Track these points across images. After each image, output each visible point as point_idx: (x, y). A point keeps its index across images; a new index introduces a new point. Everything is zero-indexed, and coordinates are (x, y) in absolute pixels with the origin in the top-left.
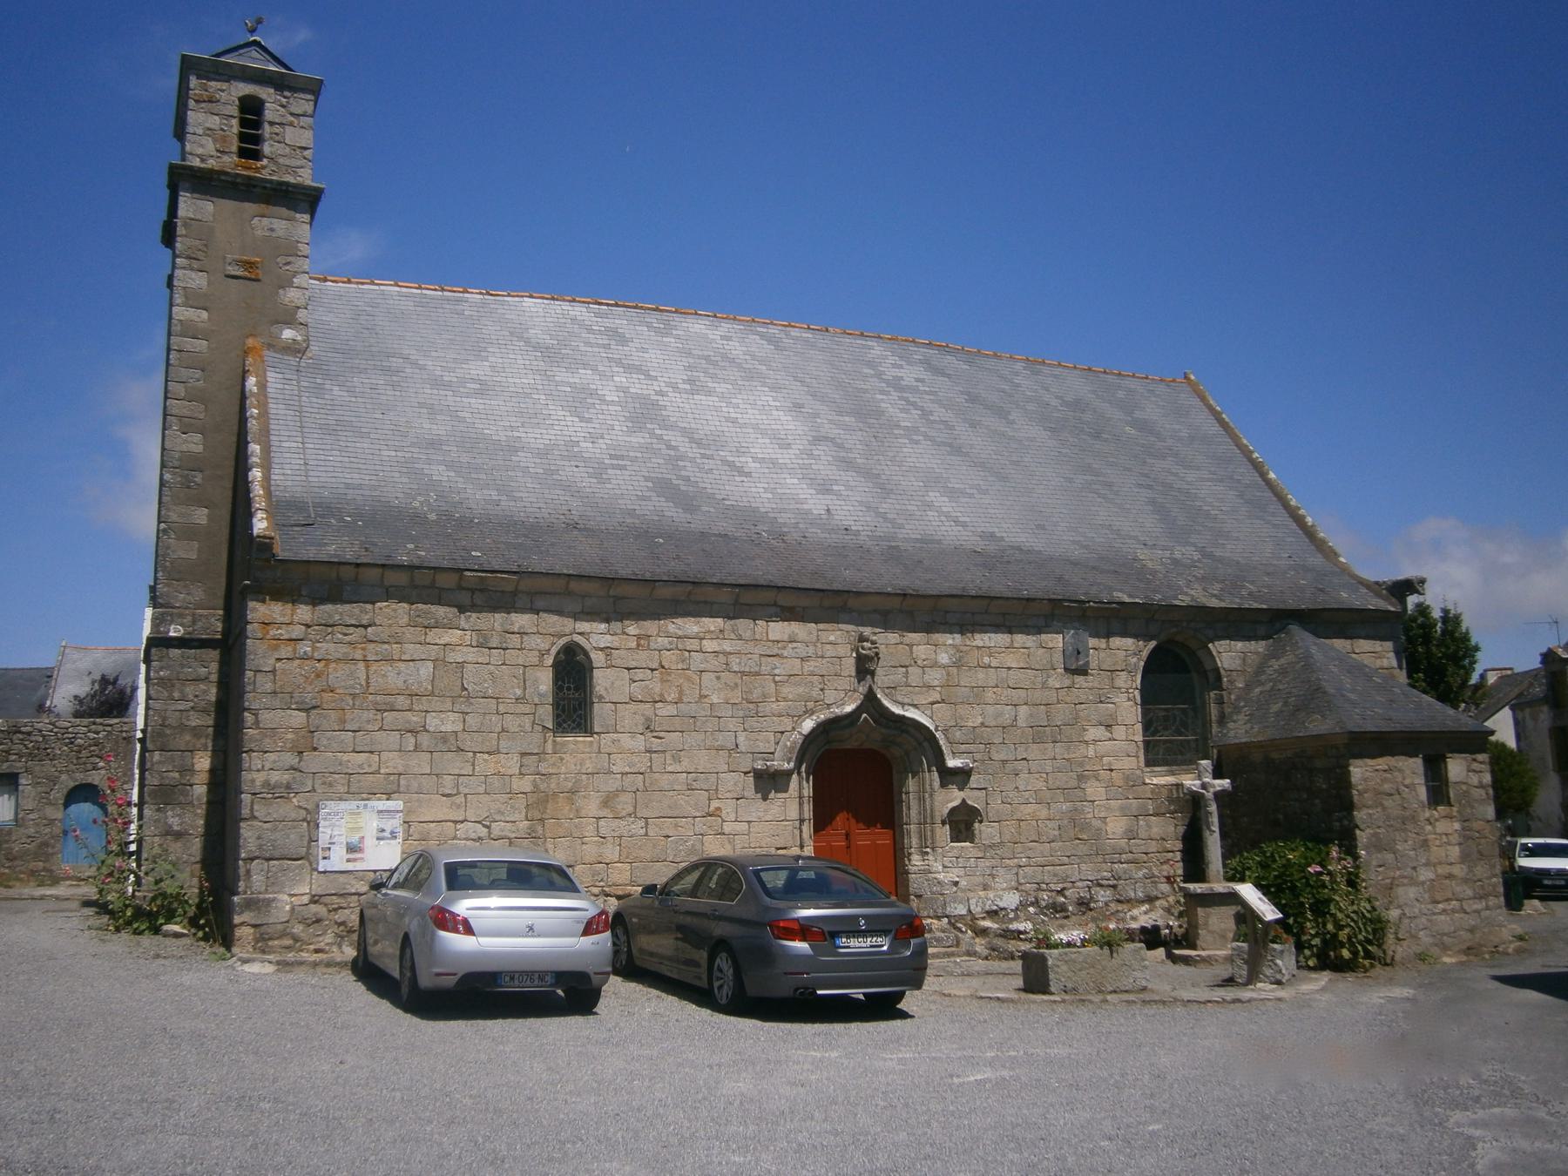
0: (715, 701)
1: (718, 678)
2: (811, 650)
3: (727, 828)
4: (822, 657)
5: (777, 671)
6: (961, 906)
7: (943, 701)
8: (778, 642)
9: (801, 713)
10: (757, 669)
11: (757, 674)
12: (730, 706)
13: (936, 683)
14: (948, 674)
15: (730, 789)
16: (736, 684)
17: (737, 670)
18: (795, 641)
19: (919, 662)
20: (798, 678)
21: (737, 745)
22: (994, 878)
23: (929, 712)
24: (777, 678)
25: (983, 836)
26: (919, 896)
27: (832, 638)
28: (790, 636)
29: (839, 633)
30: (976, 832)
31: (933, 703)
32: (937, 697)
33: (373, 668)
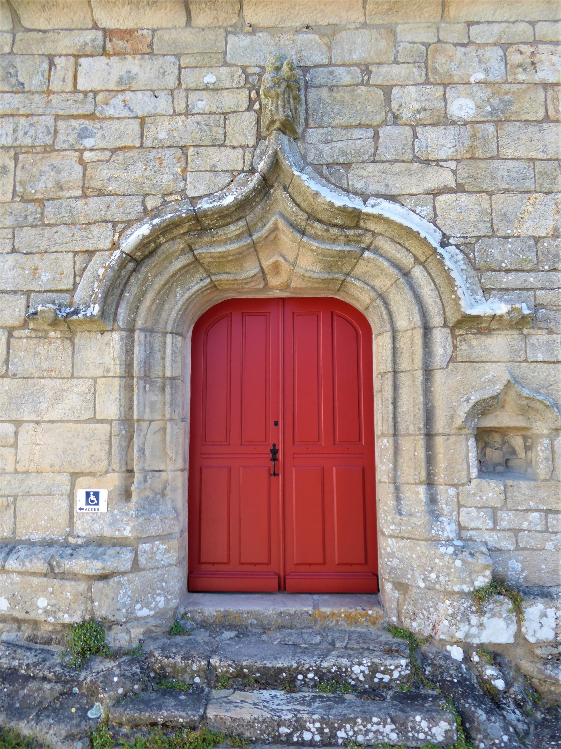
7: (460, 189)
8: (96, 93)
11: (49, 149)
24: (87, 155)
27: (210, 79)
28: (121, 81)
31: (436, 193)
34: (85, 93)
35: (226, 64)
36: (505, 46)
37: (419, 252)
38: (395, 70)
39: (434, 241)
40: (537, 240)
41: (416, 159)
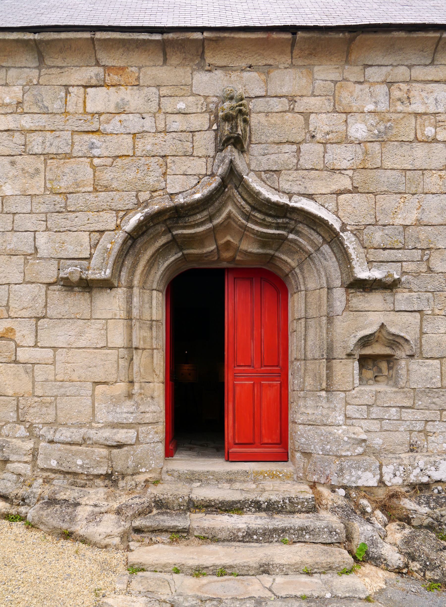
0: (9, 193)
1: (13, 163)
2: (148, 124)
3: (22, 355)
4: (166, 132)
5: (96, 152)
6: (369, 475)
7: (355, 190)
8: (100, 114)
9: (130, 206)
10: (67, 150)
11: (68, 156)
12: (28, 199)
13: (345, 164)
14: (366, 153)
15: (26, 305)
16: (37, 171)
17: (39, 151)
18: (124, 112)
19: (319, 137)
20: (127, 160)
21: (36, 249)
22: (427, 436)
23: (332, 206)
24: (96, 161)
25: (414, 377)
26: (307, 454)
27: (181, 106)
28: (117, 105)
29: (191, 99)
30: (403, 372)
31: (339, 193)
32: (347, 183)
33: (56, 262)
34: (93, 114)
35: (193, 95)
36: (390, 84)
37: (326, 236)
38: (313, 100)
39: (337, 226)
40: (405, 227)
41: (326, 169)
